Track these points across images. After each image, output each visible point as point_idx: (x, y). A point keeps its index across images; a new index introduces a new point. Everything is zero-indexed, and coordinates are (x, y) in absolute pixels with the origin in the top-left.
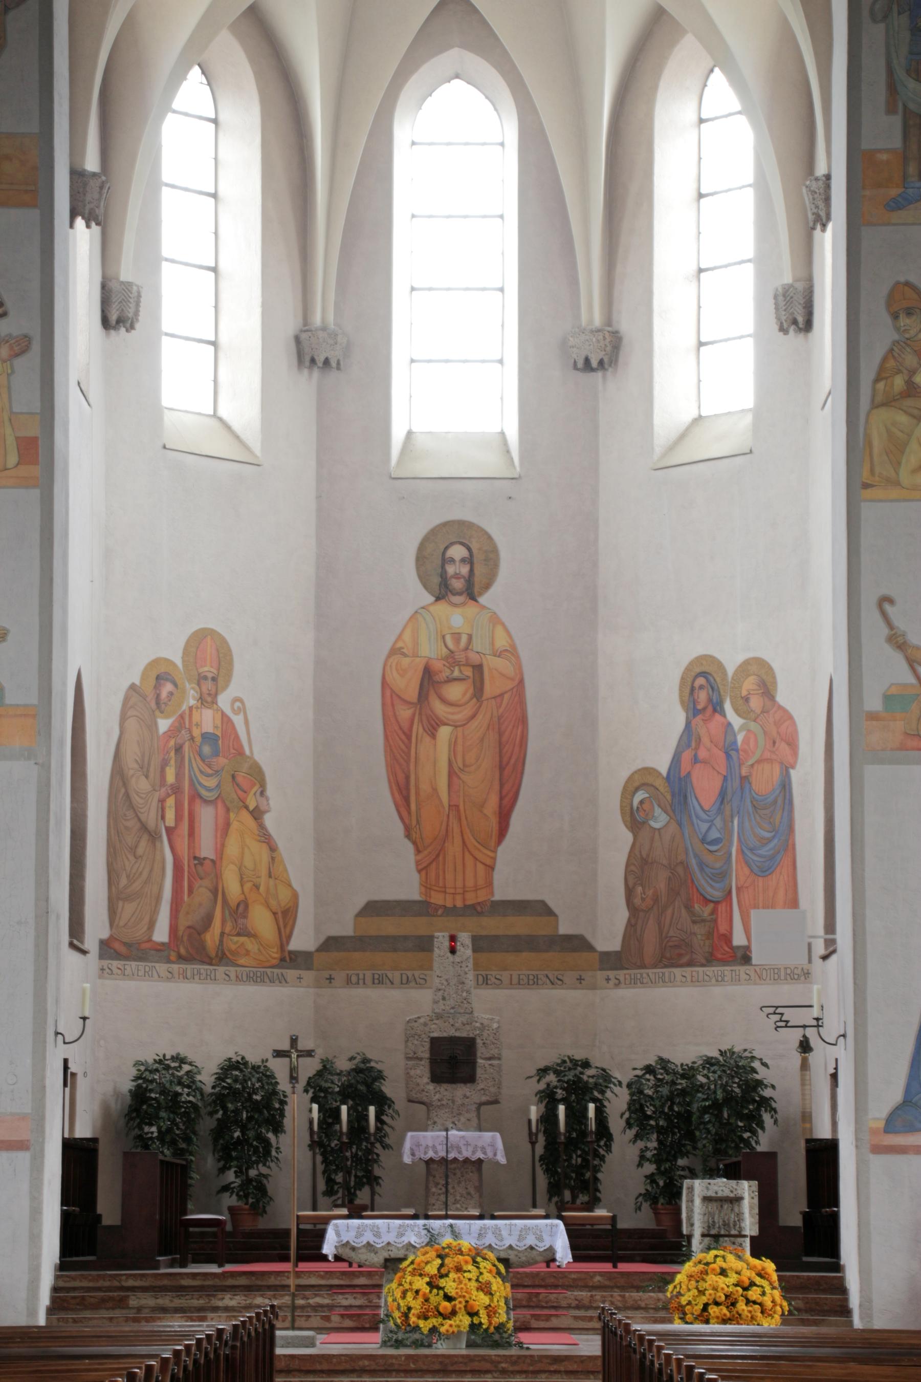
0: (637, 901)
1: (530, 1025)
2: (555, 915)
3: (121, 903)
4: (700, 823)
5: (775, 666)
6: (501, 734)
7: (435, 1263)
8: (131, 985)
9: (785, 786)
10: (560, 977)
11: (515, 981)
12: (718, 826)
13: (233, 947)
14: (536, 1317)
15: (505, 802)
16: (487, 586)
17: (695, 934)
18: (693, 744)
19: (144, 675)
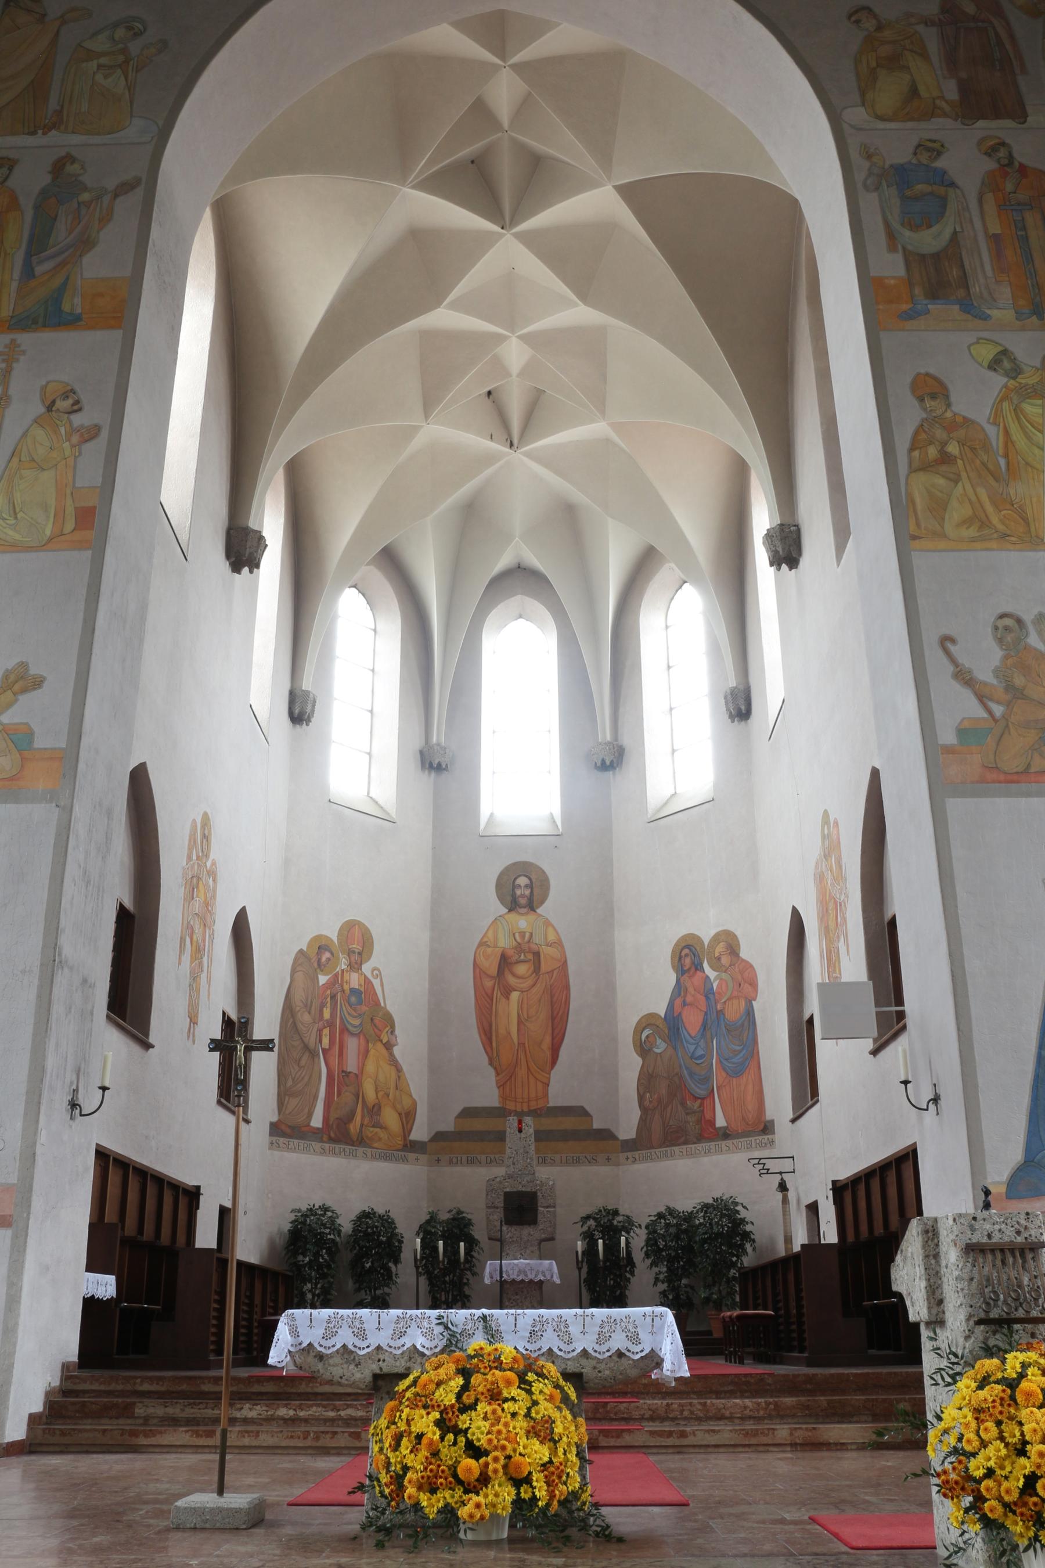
0: (647, 1103)
1: (574, 1188)
5: (738, 933)
6: (552, 997)
7: (452, 1383)
8: (293, 1156)
9: (750, 1013)
11: (564, 1160)
14: (606, 1433)
16: (542, 902)
19: (310, 944)
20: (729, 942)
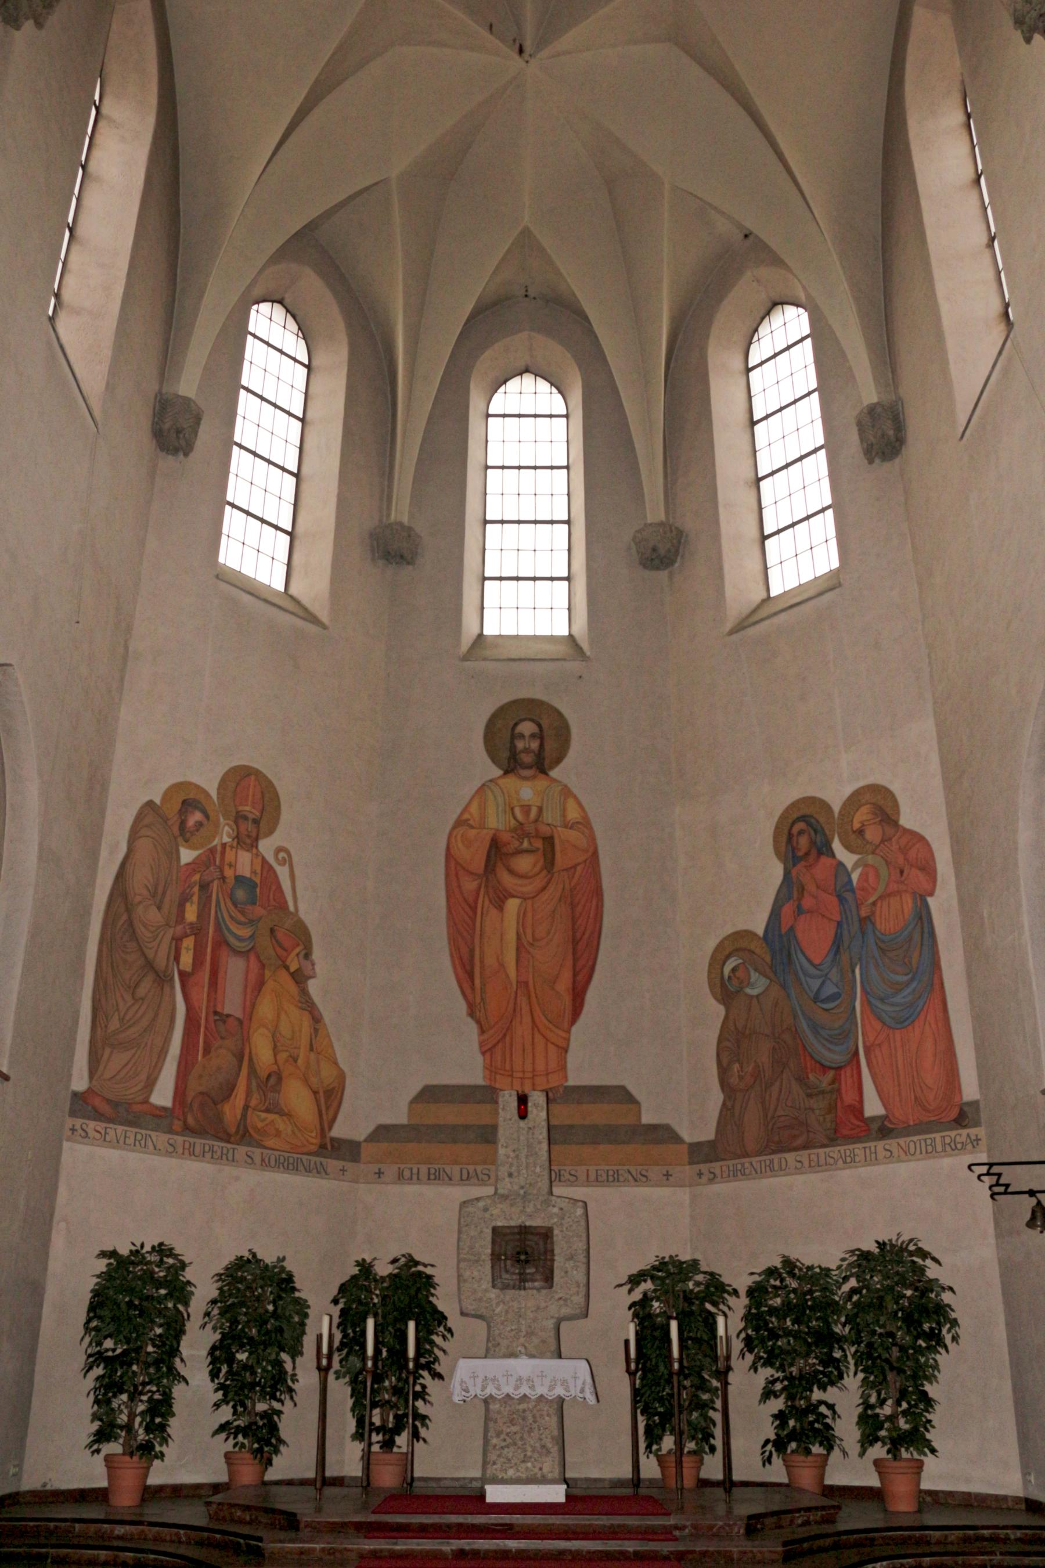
2: (636, 1102)
3: (108, 1051)
4: (808, 979)
5: (895, 788)
6: (573, 906)
8: (114, 1155)
9: (923, 918)
10: (644, 1173)
11: (592, 1177)
12: (835, 980)
13: (260, 1125)
15: (579, 978)
16: (558, 760)
17: (813, 1110)
18: (795, 895)
19: (168, 795)
20: (879, 804)
